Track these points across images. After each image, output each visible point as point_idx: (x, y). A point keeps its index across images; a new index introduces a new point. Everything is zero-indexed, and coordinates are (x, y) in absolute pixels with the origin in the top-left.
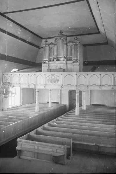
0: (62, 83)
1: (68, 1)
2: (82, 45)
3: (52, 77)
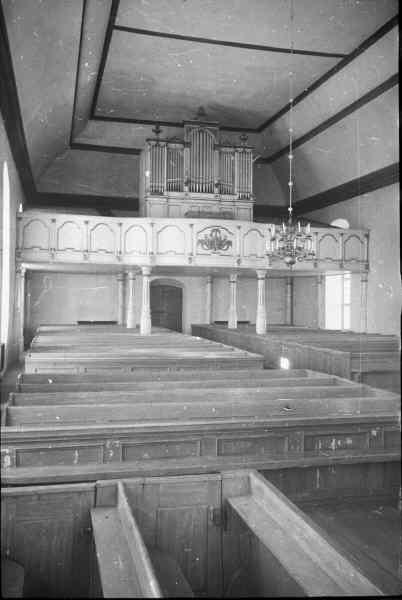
1: (257, 44)
3: (214, 234)
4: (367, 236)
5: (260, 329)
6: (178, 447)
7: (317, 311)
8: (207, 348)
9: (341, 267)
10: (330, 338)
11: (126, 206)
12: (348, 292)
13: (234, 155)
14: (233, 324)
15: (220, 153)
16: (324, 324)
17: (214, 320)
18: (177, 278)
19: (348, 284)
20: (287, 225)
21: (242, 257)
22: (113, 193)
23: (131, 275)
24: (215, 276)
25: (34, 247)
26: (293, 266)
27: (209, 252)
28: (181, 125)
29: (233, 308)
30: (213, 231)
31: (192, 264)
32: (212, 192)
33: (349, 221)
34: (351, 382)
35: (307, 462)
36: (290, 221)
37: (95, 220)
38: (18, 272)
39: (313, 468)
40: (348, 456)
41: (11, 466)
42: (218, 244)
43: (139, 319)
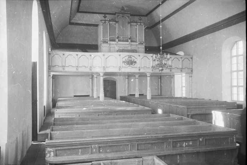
0: (140, 65)
2: (98, 25)
3: (129, 58)
4: (192, 58)
5: (149, 97)
6: (121, 147)
7: (171, 89)
8: (128, 106)
9: (181, 71)
10: (178, 100)
11: (94, 48)
12: (184, 81)
13: (136, 26)
14: (137, 96)
15: (131, 25)
16: (174, 94)
17: (129, 94)
18: (114, 77)
19: (184, 78)
20: (160, 54)
21: (140, 68)
22: (86, 43)
23: (95, 76)
24: (129, 76)
25: (55, 66)
26: (163, 71)
27: (127, 66)
28: (115, 14)
29: (137, 88)
30: (129, 57)
31: (120, 71)
32: (128, 41)
33: (184, 52)
34: (188, 118)
35: (174, 152)
36: (161, 53)
37: (80, 54)
38: (49, 76)
39: (176, 155)
40: (191, 150)
41: (54, 156)
42: (131, 63)
43: (99, 94)
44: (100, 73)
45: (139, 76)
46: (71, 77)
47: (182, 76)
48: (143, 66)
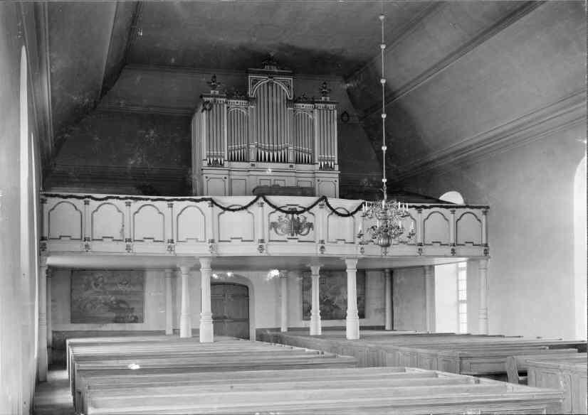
14: (284, 329)
44: (347, 262)
45: (320, 271)
46: (383, 285)
47: (458, 270)
48: (332, 238)
